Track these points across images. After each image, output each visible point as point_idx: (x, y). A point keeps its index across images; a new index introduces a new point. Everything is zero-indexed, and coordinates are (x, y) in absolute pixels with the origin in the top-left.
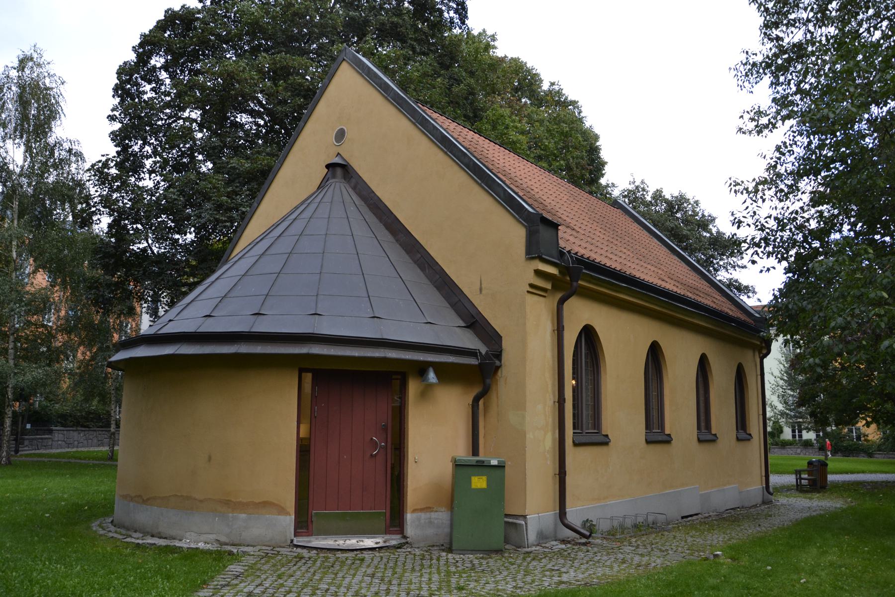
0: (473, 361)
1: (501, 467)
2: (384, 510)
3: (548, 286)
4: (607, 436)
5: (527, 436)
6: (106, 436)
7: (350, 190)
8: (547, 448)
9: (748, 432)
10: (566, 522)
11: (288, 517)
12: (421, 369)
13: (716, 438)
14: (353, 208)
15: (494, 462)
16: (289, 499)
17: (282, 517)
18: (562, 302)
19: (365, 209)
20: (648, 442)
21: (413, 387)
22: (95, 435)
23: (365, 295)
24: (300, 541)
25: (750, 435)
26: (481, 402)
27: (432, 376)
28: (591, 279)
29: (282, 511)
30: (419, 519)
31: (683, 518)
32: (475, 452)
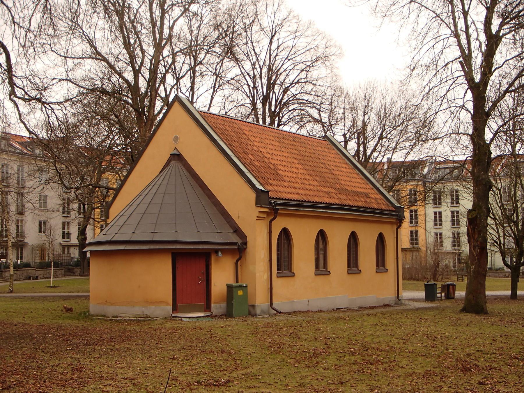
0: (236, 247)
1: (246, 286)
2: (203, 303)
3: (265, 216)
4: (294, 273)
7: (182, 167)
8: (265, 279)
12: (216, 251)
14: (184, 178)
15: (244, 285)
16: (170, 300)
18: (463, 76)
19: (190, 177)
20: (315, 275)
21: (213, 258)
23: (194, 222)
25: (387, 269)
26: (239, 262)
27: (220, 254)
28: (281, 211)
29: (168, 304)
31: (337, 309)
32: (237, 282)
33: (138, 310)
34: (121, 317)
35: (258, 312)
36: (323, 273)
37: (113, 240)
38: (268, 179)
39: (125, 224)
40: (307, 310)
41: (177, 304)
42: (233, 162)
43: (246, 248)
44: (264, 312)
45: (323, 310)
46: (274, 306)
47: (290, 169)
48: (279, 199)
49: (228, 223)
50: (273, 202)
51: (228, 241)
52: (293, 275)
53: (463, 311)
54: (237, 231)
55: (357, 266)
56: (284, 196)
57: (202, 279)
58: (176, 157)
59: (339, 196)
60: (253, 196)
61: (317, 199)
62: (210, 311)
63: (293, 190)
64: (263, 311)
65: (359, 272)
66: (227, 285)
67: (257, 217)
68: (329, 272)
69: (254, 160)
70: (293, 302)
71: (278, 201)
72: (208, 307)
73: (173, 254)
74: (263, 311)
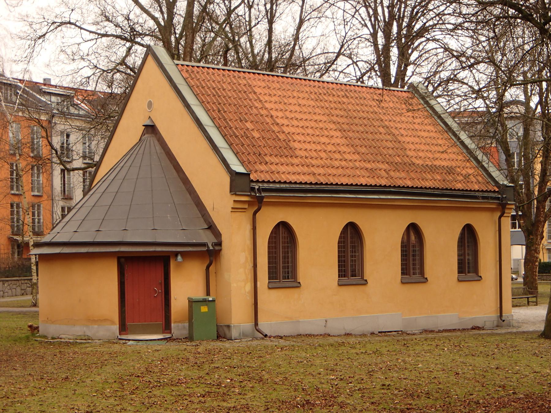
1: (213, 301)
2: (161, 322)
4: (299, 283)
5: (232, 285)
6: (28, 285)
9: (479, 275)
10: (257, 328)
11: (115, 326)
12: (176, 254)
13: (366, 283)
16: (115, 316)
17: (112, 326)
20: (339, 285)
22: (18, 284)
24: (124, 337)
25: (481, 277)
27: (179, 258)
28: (267, 198)
29: (113, 323)
30: (178, 326)
31: (379, 332)
32: (208, 294)
33: (78, 330)
34: (61, 338)
35: (234, 333)
36: (354, 283)
37: (53, 240)
38: (266, 155)
39: (72, 219)
40: (322, 333)
41: (126, 323)
42: (207, 135)
43: (221, 250)
44: (245, 335)
45: (353, 333)
46: (260, 327)
47: (315, 139)
48: (274, 182)
49: (203, 216)
50: (257, 187)
51: (194, 241)
52: (298, 286)
53: (542, 337)
54: (211, 227)
55: (422, 273)
56: (284, 178)
57: (159, 290)
58: (150, 129)
59: (392, 173)
60: (226, 179)
61: (345, 181)
62: (171, 333)
63: (305, 169)
64: (243, 334)
65: (424, 280)
66: (188, 298)
67: (232, 208)
68: (366, 280)
69: (253, 130)
70: (299, 321)
71: (266, 185)
72: (167, 327)
73: (119, 259)
74: (243, 334)
